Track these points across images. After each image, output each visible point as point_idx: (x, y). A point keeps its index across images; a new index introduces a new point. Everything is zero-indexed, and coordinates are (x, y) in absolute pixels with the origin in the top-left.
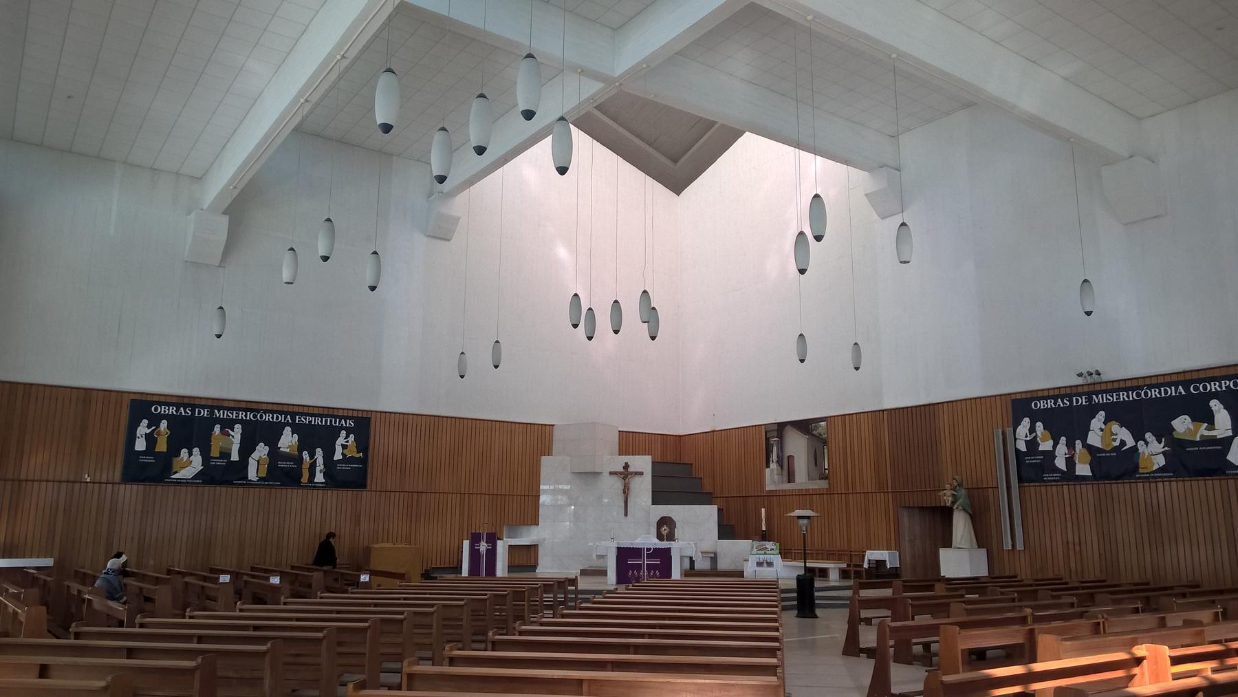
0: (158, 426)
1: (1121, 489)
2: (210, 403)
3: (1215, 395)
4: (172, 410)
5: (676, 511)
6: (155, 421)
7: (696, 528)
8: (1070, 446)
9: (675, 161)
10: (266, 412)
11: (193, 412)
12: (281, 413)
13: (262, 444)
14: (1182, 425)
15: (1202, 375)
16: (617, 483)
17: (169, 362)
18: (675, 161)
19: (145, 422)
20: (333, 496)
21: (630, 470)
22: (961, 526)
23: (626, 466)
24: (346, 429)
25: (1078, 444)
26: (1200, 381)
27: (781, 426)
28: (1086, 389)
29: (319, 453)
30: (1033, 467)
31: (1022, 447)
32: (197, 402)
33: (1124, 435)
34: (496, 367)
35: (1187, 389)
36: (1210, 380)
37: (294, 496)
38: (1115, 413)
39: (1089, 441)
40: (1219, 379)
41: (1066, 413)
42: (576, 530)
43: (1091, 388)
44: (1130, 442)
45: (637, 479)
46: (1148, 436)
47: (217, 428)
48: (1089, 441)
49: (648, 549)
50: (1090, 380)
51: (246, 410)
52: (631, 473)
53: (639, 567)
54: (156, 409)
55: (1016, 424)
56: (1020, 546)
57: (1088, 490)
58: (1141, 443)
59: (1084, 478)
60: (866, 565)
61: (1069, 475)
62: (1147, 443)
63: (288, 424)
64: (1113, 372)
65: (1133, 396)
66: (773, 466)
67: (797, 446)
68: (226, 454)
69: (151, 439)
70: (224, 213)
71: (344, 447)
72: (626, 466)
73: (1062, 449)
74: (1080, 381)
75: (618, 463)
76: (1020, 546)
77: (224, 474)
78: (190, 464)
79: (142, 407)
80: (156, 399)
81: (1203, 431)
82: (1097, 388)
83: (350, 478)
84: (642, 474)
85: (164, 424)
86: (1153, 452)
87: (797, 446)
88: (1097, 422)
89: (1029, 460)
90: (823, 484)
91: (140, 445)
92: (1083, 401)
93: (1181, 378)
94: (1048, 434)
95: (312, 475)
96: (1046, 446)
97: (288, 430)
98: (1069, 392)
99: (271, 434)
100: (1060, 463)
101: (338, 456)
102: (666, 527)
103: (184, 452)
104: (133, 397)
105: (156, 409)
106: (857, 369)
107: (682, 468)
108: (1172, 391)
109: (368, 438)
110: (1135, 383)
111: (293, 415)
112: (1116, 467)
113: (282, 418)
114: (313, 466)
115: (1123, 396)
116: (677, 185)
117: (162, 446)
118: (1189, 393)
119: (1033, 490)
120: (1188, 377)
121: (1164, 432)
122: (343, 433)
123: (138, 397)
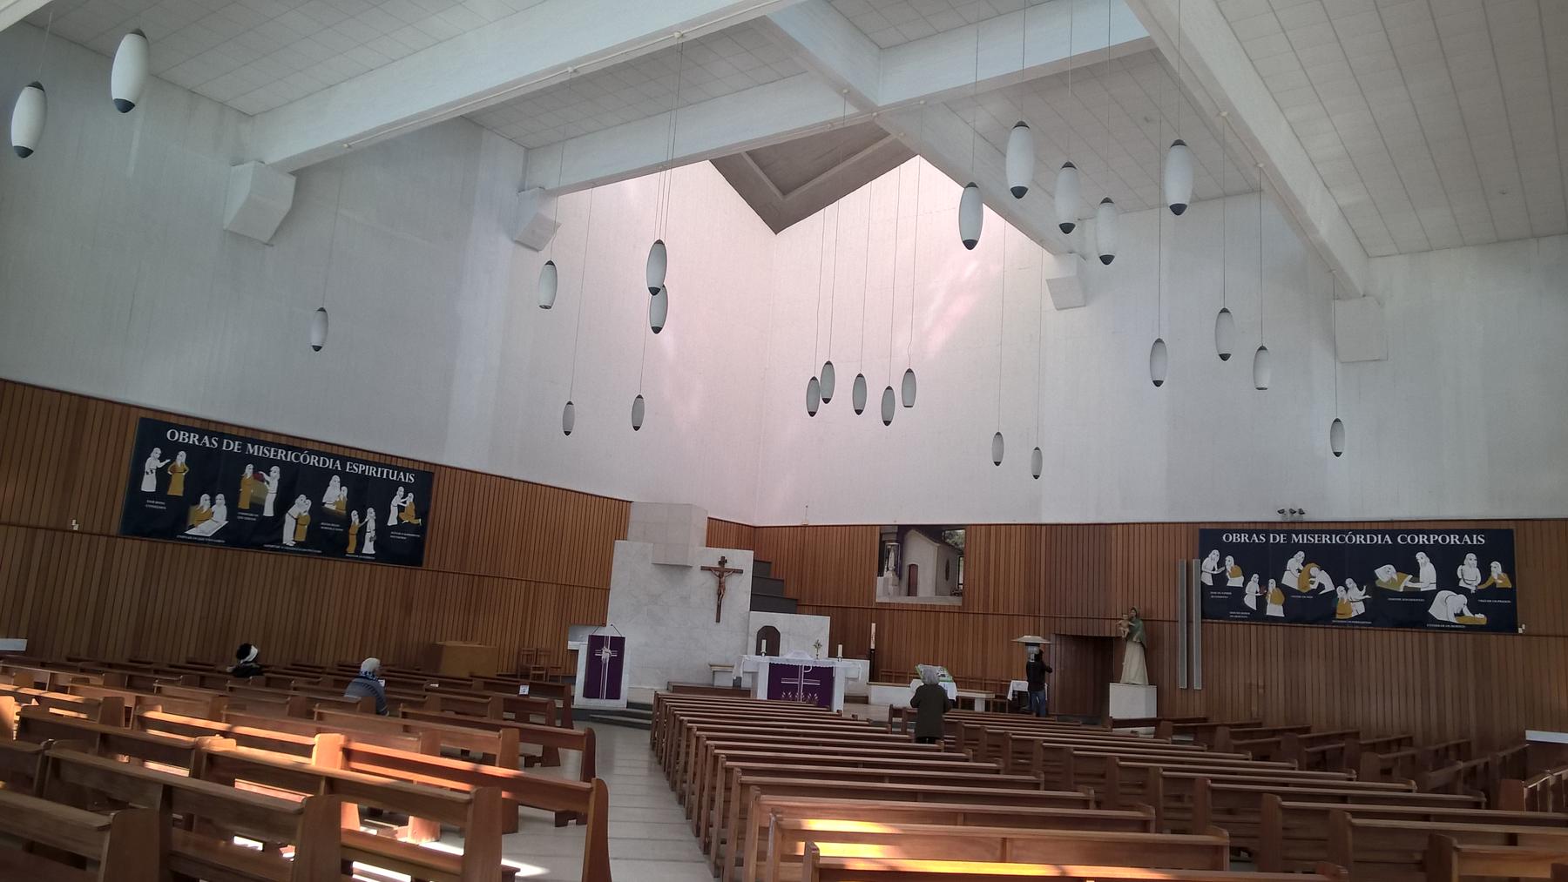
0: (174, 459)
1: (1315, 635)
2: (242, 433)
3: (1423, 548)
4: (193, 439)
5: (780, 620)
6: (170, 451)
7: (805, 638)
8: (1263, 584)
9: (785, 192)
10: (311, 452)
11: (220, 443)
12: (329, 456)
13: (303, 497)
14: (1385, 574)
15: (1411, 527)
16: (710, 581)
17: (187, 372)
18: (785, 192)
19: (157, 452)
20: (384, 571)
21: (727, 566)
22: (1133, 660)
23: (723, 561)
24: (405, 485)
25: (1272, 583)
26: (1408, 532)
27: (903, 530)
28: (1285, 527)
29: (371, 513)
30: (1220, 604)
31: (1209, 581)
32: (227, 430)
33: (1322, 578)
34: (637, 428)
35: (1394, 539)
36: (1418, 532)
37: (337, 567)
38: (1315, 555)
39: (1285, 581)
40: (1428, 532)
41: (1262, 550)
42: (673, 631)
43: (1291, 527)
44: (1329, 587)
45: (735, 577)
46: (1349, 582)
47: (249, 469)
48: (1285, 581)
49: (807, 668)
50: (1289, 518)
51: (288, 448)
52: (729, 571)
53: (794, 688)
54: (173, 435)
55: (1204, 555)
56: (1197, 685)
57: (1279, 632)
58: (1340, 588)
59: (1275, 619)
60: (1010, 697)
61: (1259, 615)
62: (1347, 589)
63: (336, 472)
64: (1316, 513)
65: (1336, 539)
66: (889, 574)
67: (923, 555)
68: (258, 507)
69: (163, 476)
70: (293, 173)
71: (401, 509)
72: (723, 561)
73: (1253, 587)
74: (1278, 518)
75: (713, 556)
76: (1197, 685)
77: (251, 533)
78: (211, 517)
79: (155, 429)
80: (173, 420)
81: (1407, 582)
82: (1298, 527)
83: (402, 550)
84: (741, 572)
85: (182, 457)
86: (1353, 599)
87: (923, 555)
88: (1295, 563)
89: (1214, 595)
90: (956, 601)
91: (149, 484)
92: (1281, 539)
93: (1389, 527)
94: (1239, 569)
95: (360, 544)
96: (1236, 581)
97: (336, 479)
98: (1267, 528)
99: (314, 483)
100: (1250, 601)
101: (392, 521)
102: (770, 639)
103: (205, 498)
104: (143, 414)
105: (173, 435)
106: (1036, 477)
107: (786, 567)
108: (1378, 539)
109: (429, 499)
110: (1339, 527)
111: (344, 460)
112: (1312, 610)
113: (329, 463)
114: (362, 531)
115: (1325, 539)
116: (778, 222)
117: (177, 488)
118: (1398, 542)
119: (1216, 627)
120: (1396, 527)
121: (1366, 579)
122: (401, 489)
123: (150, 415)
